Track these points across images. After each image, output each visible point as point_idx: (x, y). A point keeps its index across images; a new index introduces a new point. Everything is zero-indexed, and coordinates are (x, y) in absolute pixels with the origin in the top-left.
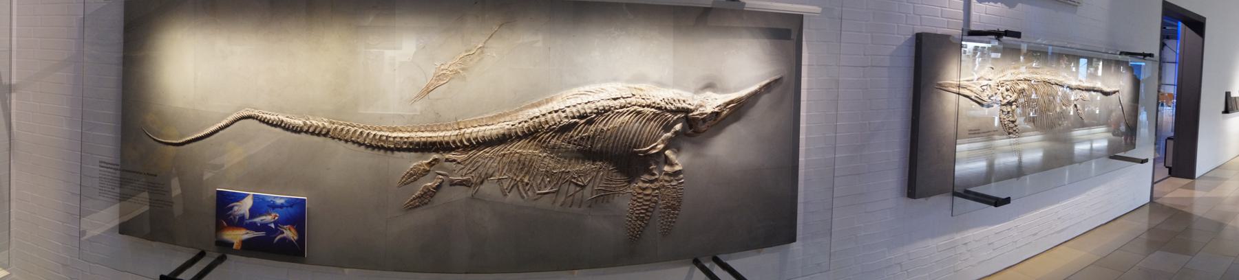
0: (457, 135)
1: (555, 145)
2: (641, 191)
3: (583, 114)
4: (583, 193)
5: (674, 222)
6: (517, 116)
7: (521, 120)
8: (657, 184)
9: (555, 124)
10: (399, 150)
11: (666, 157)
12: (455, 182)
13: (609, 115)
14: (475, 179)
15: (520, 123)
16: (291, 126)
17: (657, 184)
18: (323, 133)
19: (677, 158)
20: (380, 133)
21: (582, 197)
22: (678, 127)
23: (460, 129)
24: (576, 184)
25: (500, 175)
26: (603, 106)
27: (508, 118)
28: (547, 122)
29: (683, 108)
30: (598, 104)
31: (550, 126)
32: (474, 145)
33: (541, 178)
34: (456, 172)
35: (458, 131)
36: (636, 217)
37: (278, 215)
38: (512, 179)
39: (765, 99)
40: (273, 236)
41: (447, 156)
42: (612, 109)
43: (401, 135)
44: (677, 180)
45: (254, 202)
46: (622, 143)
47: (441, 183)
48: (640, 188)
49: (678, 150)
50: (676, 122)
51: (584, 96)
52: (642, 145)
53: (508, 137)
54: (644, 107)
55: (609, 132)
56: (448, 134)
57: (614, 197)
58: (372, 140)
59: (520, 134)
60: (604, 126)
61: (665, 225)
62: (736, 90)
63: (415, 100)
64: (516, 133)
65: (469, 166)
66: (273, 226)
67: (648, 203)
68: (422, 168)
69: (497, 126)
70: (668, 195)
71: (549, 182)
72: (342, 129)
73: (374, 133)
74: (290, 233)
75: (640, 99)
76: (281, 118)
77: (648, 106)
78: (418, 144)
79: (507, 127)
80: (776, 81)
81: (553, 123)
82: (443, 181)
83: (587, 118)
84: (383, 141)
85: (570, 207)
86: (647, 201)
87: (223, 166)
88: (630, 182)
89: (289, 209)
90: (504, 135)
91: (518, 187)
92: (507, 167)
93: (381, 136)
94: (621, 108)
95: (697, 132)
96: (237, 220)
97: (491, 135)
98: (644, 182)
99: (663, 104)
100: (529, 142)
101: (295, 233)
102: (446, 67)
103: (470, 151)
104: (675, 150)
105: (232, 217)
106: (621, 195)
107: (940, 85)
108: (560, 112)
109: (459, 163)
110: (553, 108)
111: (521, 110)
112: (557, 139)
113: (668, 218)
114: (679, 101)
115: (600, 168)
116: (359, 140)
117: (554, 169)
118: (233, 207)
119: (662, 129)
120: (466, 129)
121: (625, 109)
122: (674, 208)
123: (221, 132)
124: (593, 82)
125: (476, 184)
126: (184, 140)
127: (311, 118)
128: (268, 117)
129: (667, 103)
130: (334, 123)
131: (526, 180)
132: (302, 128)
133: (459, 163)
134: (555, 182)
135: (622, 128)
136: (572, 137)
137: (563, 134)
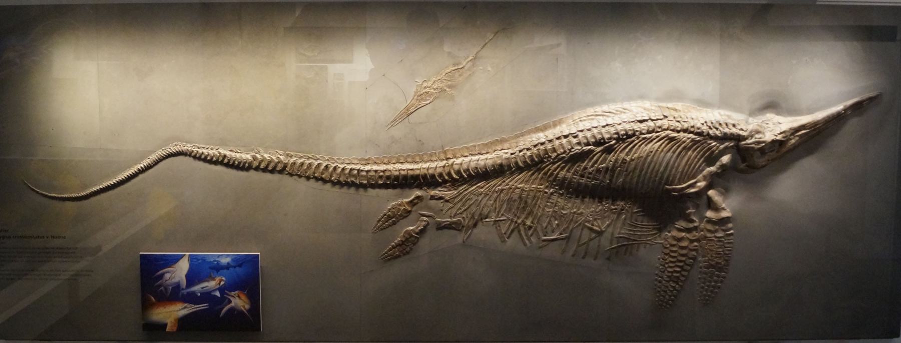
0: (444, 167)
1: (564, 179)
2: (675, 243)
3: (600, 140)
4: (599, 241)
5: (719, 287)
6: (517, 143)
7: (523, 148)
8: (695, 235)
9: (565, 152)
10: (373, 186)
11: (709, 199)
12: (443, 225)
13: (633, 141)
14: (467, 221)
15: (520, 151)
16: (237, 162)
17: (695, 235)
18: (278, 169)
19: (724, 201)
20: (349, 167)
21: (599, 246)
22: (726, 159)
23: (447, 159)
24: (591, 229)
25: (497, 216)
26: (625, 130)
27: (506, 145)
28: (554, 150)
29: (732, 134)
30: (619, 128)
31: (558, 155)
32: (465, 179)
33: (548, 220)
34: (444, 212)
35: (445, 162)
36: (668, 277)
37: (224, 278)
38: (512, 221)
39: (853, 125)
40: (220, 307)
41: (433, 193)
42: (637, 133)
43: (375, 167)
44: (724, 231)
45: (191, 265)
46: (650, 178)
47: (425, 227)
48: (674, 238)
49: (725, 192)
50: (723, 153)
51: (601, 118)
52: (677, 181)
53: (506, 168)
54: (678, 132)
55: (633, 163)
56: (433, 165)
57: (638, 247)
58: (340, 175)
59: (521, 164)
60: (627, 155)
61: (706, 291)
62: (810, 111)
63: (394, 122)
64: (516, 163)
65: (459, 205)
66: (218, 294)
67: (684, 259)
68: (402, 208)
69: (493, 155)
70: (711, 251)
71: (558, 225)
72: (302, 164)
73: (342, 166)
74: (239, 302)
75: (674, 122)
76: (223, 152)
77: (685, 131)
78: (397, 178)
79: (505, 156)
80: (871, 99)
81: (562, 151)
82: (428, 224)
83: (606, 145)
84: (354, 176)
85: (583, 258)
86: (683, 255)
87: (99, 249)
88: (660, 230)
89: (238, 269)
90: (501, 165)
91: (519, 231)
92: (505, 206)
93: (351, 170)
94: (649, 132)
95: (752, 168)
96: (168, 294)
97: (485, 165)
98: (680, 230)
99: (705, 128)
100: (533, 174)
101: (247, 300)
102: (430, 83)
103: (460, 186)
104: (723, 191)
105: (162, 288)
106: (648, 246)
108: (570, 137)
109: (447, 201)
110: (562, 132)
111: (522, 135)
112: (568, 171)
113: (710, 282)
114: (727, 124)
115: (622, 210)
116: (323, 176)
117: (563, 209)
118: (163, 274)
119: (703, 162)
120: (454, 160)
121: (654, 135)
122: (720, 268)
123: (141, 176)
124: (613, 101)
125: (468, 228)
126: (88, 192)
127: (262, 151)
128: (205, 152)
129: (710, 128)
130: (291, 156)
131: (528, 223)
132: (250, 164)
133: (447, 201)
134: (565, 226)
135: (650, 158)
136: (585, 168)
137: (574, 164)
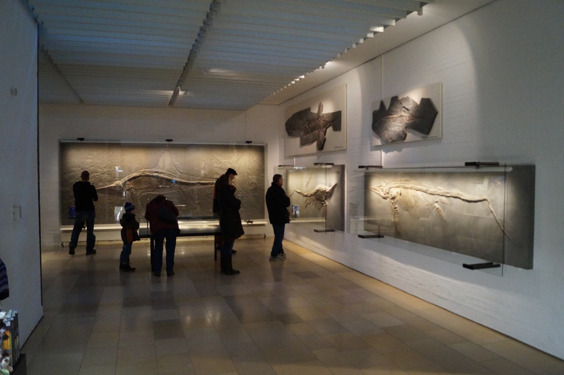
39: (336, 189)
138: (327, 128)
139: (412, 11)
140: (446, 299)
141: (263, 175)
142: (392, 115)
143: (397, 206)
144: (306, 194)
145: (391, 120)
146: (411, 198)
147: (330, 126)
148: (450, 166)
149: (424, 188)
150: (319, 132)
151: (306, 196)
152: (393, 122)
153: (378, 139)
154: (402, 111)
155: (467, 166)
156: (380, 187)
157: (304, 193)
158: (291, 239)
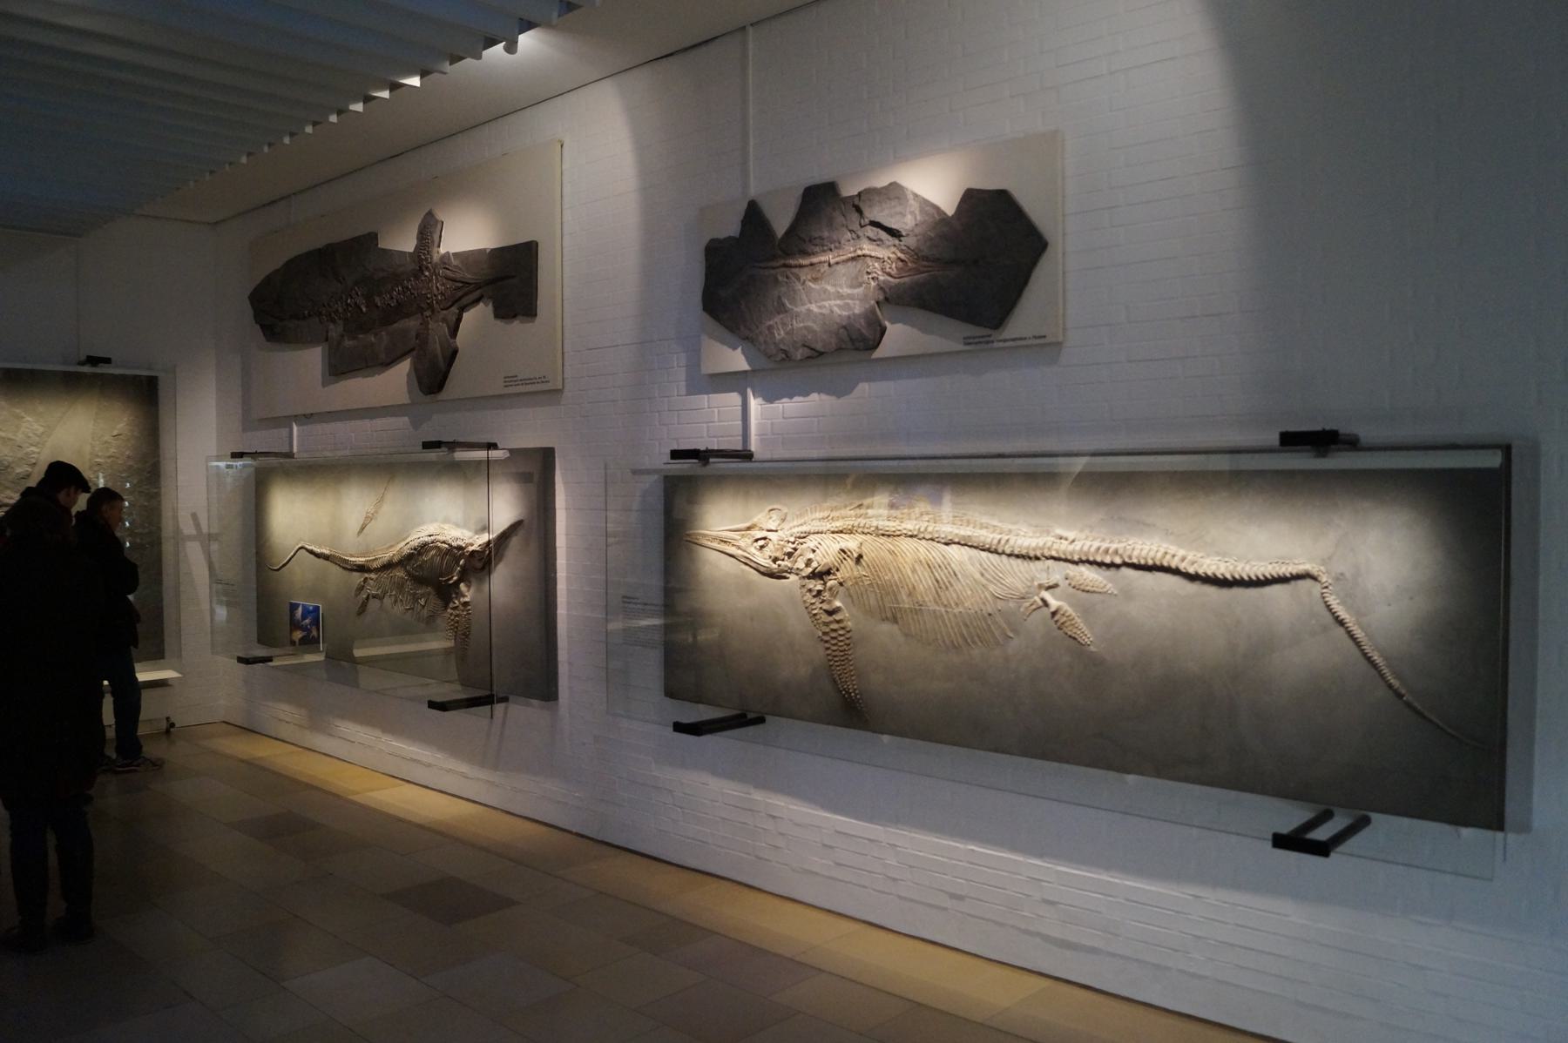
39: (515, 542)
107: (689, 535)
138: (463, 309)
139: (461, 54)
140: (1093, 950)
141: (156, 491)
142: (805, 253)
143: (838, 603)
144: (361, 560)
145: (805, 274)
146: (914, 571)
147: (476, 301)
148: (1155, 446)
149: (988, 537)
150: (425, 324)
151: (361, 568)
152: (815, 280)
153: (735, 348)
154: (866, 240)
155: (425, 450)
156: (752, 532)
157: (352, 556)
158: (285, 731)
